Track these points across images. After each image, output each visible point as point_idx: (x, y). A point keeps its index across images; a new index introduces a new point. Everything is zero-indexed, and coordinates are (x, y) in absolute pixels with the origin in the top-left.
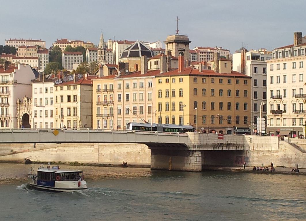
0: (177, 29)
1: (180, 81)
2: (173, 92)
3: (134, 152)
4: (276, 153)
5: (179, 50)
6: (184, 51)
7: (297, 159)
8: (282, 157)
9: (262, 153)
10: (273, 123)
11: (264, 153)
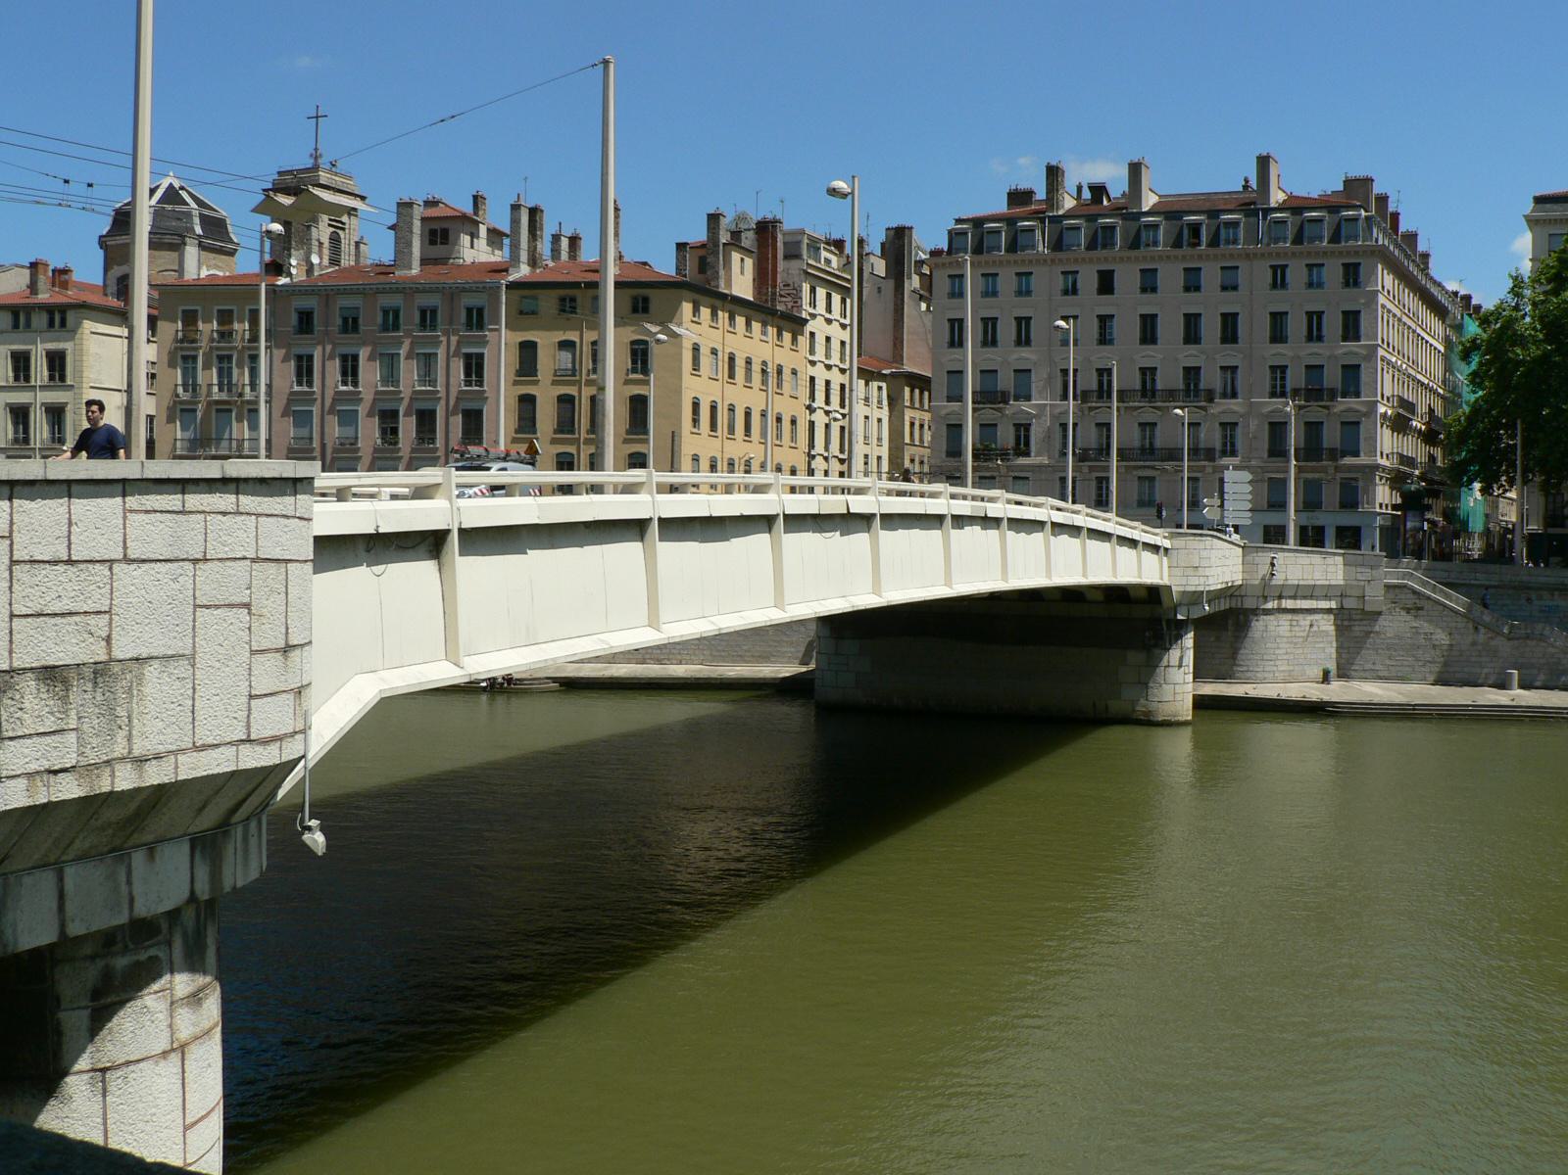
0: (316, 149)
2: (730, 358)
4: (1365, 622)
6: (343, 229)
7: (1480, 648)
8: (1400, 638)
9: (1308, 623)
10: (1384, 490)
11: (1315, 623)
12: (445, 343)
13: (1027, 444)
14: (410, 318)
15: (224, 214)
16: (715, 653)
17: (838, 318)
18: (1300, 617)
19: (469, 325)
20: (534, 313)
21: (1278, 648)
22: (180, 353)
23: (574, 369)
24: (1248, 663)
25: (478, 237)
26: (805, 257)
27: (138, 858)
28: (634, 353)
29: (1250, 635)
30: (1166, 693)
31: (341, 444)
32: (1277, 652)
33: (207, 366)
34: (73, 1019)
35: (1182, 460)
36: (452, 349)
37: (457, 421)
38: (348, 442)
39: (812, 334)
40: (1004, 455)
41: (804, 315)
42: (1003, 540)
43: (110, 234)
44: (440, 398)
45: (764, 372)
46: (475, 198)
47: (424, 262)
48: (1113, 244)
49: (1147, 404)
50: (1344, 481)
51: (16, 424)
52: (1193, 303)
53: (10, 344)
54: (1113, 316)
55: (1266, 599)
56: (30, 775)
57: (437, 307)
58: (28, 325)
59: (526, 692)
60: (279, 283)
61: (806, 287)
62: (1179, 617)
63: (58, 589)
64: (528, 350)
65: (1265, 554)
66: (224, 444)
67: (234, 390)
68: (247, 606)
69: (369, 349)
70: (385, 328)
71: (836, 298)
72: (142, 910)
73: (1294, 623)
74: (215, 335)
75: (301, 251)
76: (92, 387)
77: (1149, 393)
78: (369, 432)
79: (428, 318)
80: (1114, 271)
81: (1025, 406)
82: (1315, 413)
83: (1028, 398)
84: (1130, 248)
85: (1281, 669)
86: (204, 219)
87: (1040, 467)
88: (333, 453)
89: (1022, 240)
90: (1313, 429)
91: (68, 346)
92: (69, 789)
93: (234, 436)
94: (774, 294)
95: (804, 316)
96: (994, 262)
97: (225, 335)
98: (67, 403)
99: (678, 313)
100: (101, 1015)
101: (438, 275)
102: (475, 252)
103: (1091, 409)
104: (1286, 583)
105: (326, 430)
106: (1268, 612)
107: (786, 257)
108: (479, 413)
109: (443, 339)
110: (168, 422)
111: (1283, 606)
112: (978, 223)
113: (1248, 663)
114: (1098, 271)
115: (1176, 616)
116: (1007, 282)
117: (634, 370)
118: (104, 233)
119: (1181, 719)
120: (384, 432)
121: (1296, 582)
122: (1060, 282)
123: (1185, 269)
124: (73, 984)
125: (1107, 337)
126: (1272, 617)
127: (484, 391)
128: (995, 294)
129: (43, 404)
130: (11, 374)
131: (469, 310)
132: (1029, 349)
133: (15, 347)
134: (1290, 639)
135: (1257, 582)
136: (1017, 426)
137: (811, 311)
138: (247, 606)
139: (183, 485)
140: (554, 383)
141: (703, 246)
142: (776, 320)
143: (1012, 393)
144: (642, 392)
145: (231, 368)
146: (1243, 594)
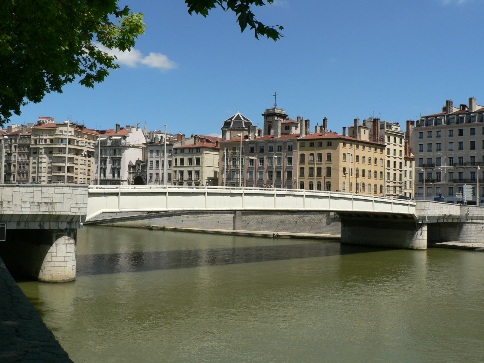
0: (275, 103)
1: (311, 146)
3: (289, 221)
5: (267, 123)
9: (482, 227)
12: (283, 155)
13: (440, 178)
14: (266, 150)
15: (251, 121)
16: (333, 231)
17: (399, 144)
18: (479, 225)
19: (289, 150)
20: (304, 147)
21: (472, 233)
22: (232, 158)
23: (313, 161)
24: (462, 237)
25: (298, 127)
26: (385, 128)
27: (60, 223)
28: (328, 156)
29: (463, 229)
30: (417, 242)
31: (260, 180)
32: (471, 234)
33: (230, 161)
34: (54, 239)
35: (477, 182)
36: (285, 156)
37: (286, 174)
38: (261, 179)
39: (389, 149)
40: (433, 181)
41: (385, 144)
42: (352, 202)
43: (223, 127)
44: (282, 168)
45: (370, 160)
46: (297, 117)
47: (282, 134)
48: (463, 122)
49: (472, 167)
50: (300, 188)
51: (189, 175)
52: (461, 139)
53: (189, 156)
54: (463, 142)
55: (467, 220)
56: (43, 211)
57: (273, 146)
58: (192, 152)
59: (282, 238)
60: (246, 141)
61: (386, 137)
62: (419, 222)
63: (47, 195)
64: (302, 156)
65: (466, 208)
66: (234, 179)
67: (236, 166)
68: (71, 198)
69: (266, 156)
70: (270, 151)
71: (398, 139)
72: (60, 228)
73: (477, 226)
74: (232, 154)
75: (253, 133)
76: (206, 166)
77: (461, 164)
78: (266, 177)
79: (279, 148)
80: (463, 129)
81: (439, 168)
82: (429, 170)
83: (440, 165)
84: (468, 123)
85: (473, 239)
86: (245, 123)
87: (443, 184)
88: (258, 182)
89: (439, 122)
90: (429, 174)
91: (200, 156)
92: (47, 213)
93: (236, 178)
94: (378, 138)
95: (385, 144)
96: (440, 127)
97: (234, 153)
98: (200, 170)
99: (338, 146)
100: (57, 239)
101: (286, 138)
102: (295, 131)
103: (457, 168)
104: (473, 215)
105: (256, 176)
106: (468, 223)
107: (381, 129)
108: (291, 172)
109: (283, 153)
110: (221, 174)
111: (473, 222)
112: (427, 117)
113: (462, 237)
114: (459, 130)
115: (418, 222)
116: (434, 133)
117: (328, 161)
118: (222, 127)
119: (421, 248)
120: (269, 176)
121: (477, 215)
122: (448, 133)
123: (471, 129)
124: (54, 235)
125: (462, 148)
126: (469, 225)
127: (292, 166)
128: (431, 137)
129: (195, 170)
130: (188, 163)
131: (289, 146)
132: (422, 153)
133: (189, 157)
134: (475, 231)
135: (464, 215)
136: (437, 173)
137: (388, 143)
138: (71, 198)
139: (70, 186)
140: (309, 164)
141: (353, 127)
142: (374, 146)
143: (436, 164)
144: (330, 166)
145: (235, 161)
146: (461, 218)
